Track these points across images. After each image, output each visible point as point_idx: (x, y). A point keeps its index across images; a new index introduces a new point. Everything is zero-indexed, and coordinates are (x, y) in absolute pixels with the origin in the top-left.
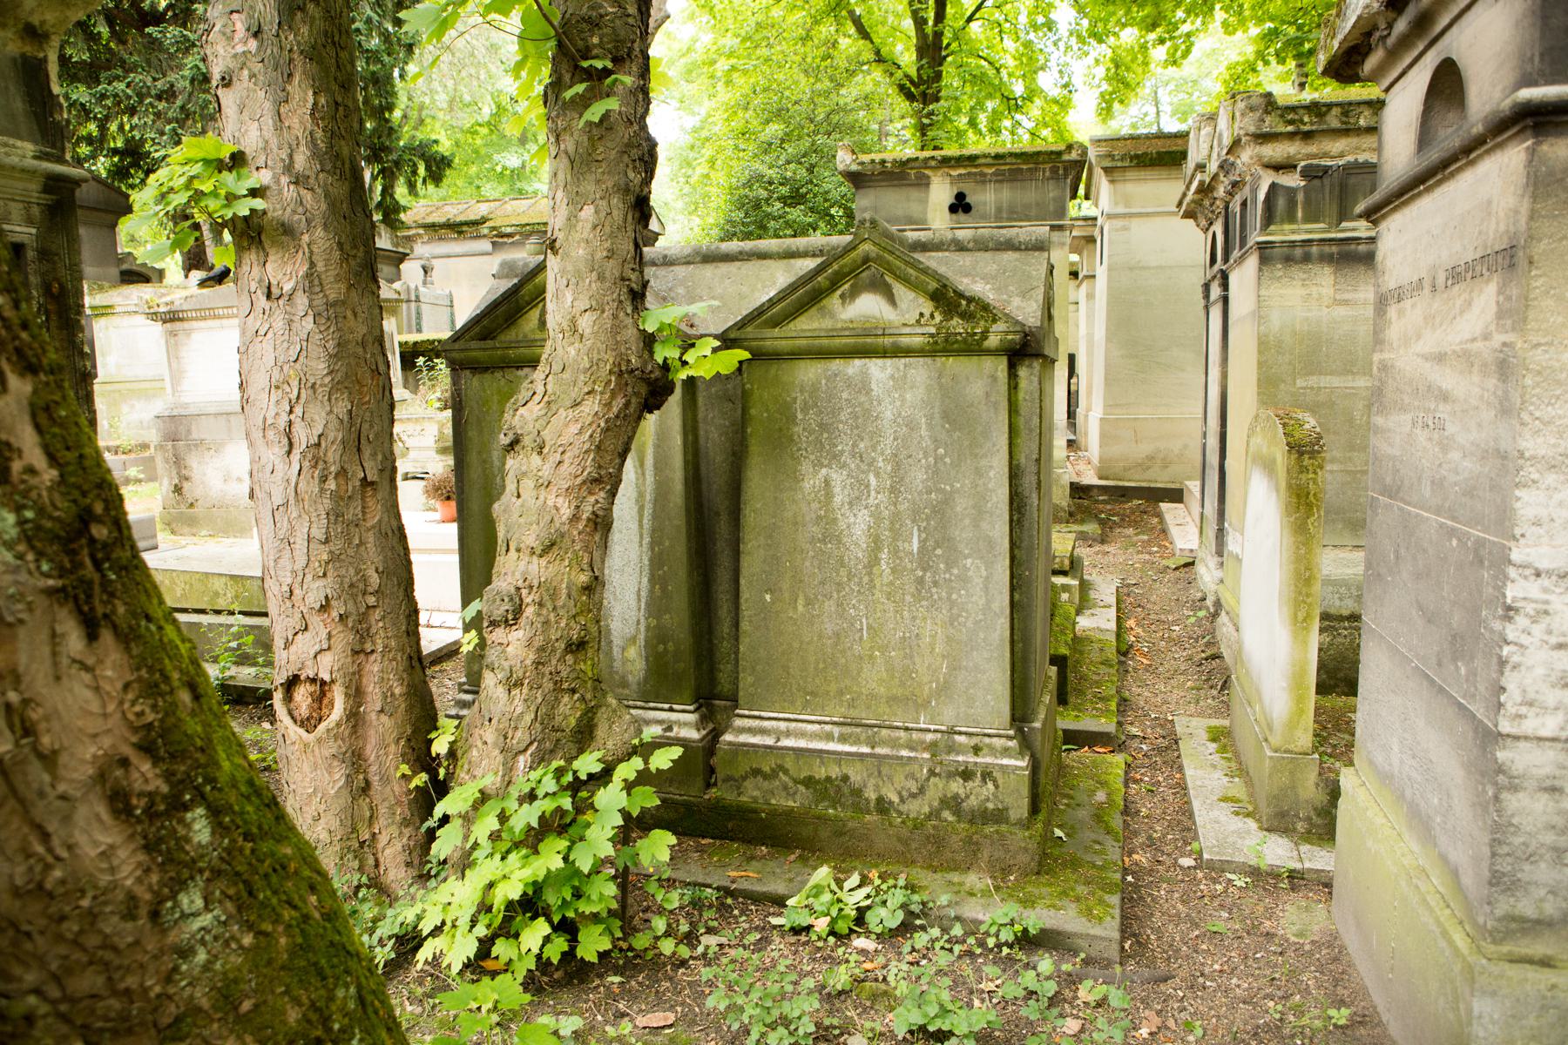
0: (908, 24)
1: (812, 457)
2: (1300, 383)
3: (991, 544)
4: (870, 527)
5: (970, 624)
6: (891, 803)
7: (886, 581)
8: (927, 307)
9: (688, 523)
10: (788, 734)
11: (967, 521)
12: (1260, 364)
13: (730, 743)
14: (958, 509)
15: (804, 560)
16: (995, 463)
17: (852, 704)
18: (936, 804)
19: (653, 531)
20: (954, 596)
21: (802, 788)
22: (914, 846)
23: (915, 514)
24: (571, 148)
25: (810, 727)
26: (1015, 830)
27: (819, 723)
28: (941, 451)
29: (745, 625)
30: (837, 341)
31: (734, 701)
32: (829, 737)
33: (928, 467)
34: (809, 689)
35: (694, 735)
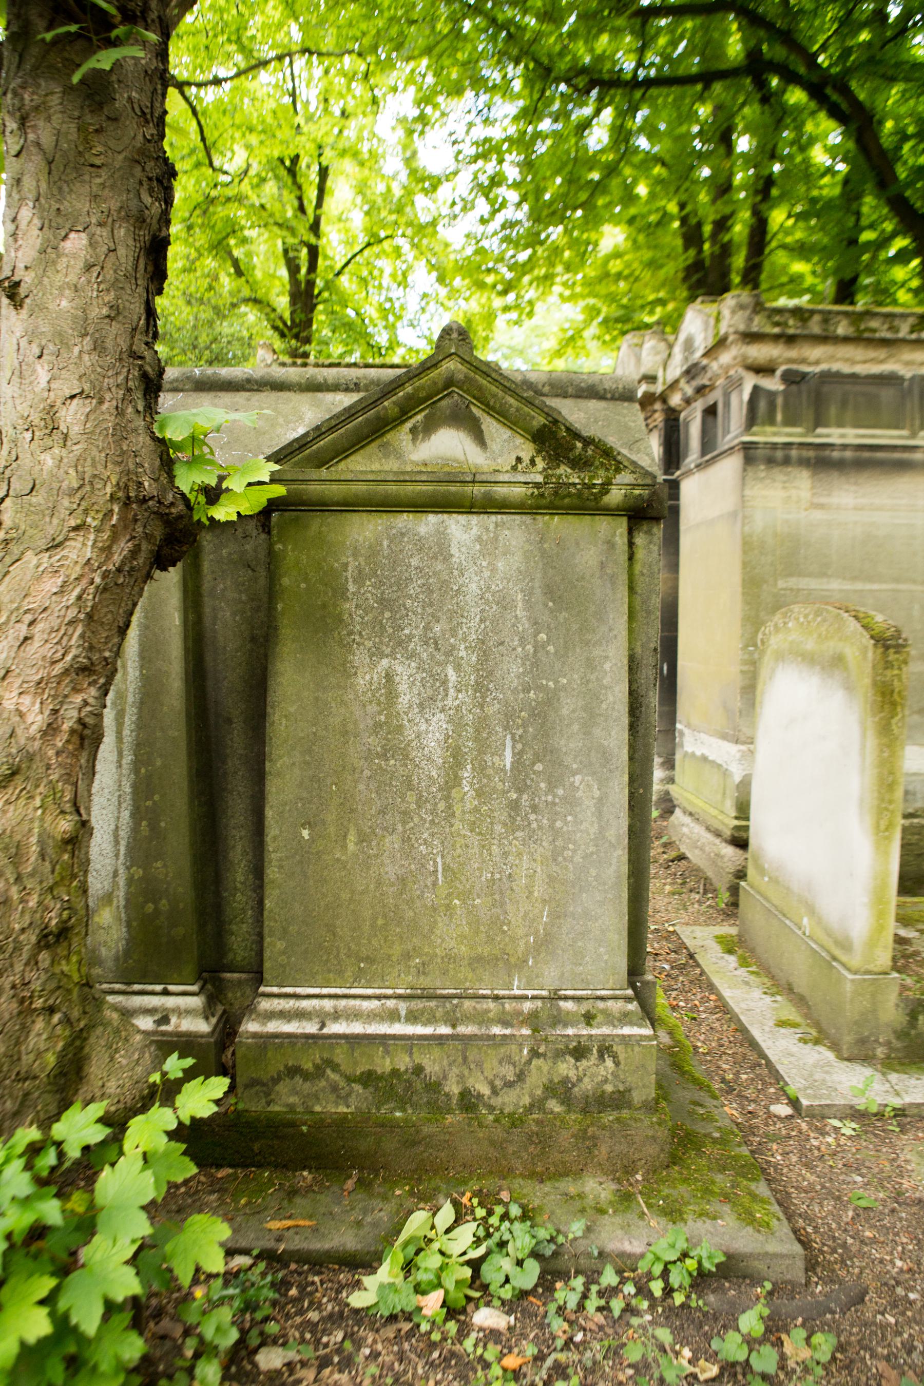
0: (284, 273)
1: (369, 644)
2: (781, 584)
3: (606, 756)
4: (447, 737)
5: (578, 859)
6: (480, 1096)
7: (468, 806)
8: (526, 450)
9: (188, 732)
10: (336, 1016)
11: (576, 727)
12: (745, 564)
13: (255, 1035)
14: (565, 711)
15: (356, 782)
16: (611, 652)
17: (422, 971)
18: (539, 1092)
19: (138, 746)
20: (558, 824)
21: (358, 1088)
22: (511, 1149)
23: (509, 717)
24: (47, 140)
25: (366, 1005)
26: (640, 1115)
27: (378, 997)
28: (543, 636)
29: (272, 873)
30: (410, 488)
31: (259, 977)
32: (393, 1016)
33: (526, 657)
34: (364, 952)
35: (202, 1026)
